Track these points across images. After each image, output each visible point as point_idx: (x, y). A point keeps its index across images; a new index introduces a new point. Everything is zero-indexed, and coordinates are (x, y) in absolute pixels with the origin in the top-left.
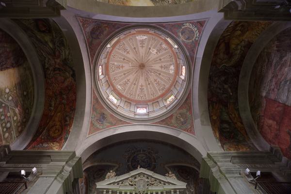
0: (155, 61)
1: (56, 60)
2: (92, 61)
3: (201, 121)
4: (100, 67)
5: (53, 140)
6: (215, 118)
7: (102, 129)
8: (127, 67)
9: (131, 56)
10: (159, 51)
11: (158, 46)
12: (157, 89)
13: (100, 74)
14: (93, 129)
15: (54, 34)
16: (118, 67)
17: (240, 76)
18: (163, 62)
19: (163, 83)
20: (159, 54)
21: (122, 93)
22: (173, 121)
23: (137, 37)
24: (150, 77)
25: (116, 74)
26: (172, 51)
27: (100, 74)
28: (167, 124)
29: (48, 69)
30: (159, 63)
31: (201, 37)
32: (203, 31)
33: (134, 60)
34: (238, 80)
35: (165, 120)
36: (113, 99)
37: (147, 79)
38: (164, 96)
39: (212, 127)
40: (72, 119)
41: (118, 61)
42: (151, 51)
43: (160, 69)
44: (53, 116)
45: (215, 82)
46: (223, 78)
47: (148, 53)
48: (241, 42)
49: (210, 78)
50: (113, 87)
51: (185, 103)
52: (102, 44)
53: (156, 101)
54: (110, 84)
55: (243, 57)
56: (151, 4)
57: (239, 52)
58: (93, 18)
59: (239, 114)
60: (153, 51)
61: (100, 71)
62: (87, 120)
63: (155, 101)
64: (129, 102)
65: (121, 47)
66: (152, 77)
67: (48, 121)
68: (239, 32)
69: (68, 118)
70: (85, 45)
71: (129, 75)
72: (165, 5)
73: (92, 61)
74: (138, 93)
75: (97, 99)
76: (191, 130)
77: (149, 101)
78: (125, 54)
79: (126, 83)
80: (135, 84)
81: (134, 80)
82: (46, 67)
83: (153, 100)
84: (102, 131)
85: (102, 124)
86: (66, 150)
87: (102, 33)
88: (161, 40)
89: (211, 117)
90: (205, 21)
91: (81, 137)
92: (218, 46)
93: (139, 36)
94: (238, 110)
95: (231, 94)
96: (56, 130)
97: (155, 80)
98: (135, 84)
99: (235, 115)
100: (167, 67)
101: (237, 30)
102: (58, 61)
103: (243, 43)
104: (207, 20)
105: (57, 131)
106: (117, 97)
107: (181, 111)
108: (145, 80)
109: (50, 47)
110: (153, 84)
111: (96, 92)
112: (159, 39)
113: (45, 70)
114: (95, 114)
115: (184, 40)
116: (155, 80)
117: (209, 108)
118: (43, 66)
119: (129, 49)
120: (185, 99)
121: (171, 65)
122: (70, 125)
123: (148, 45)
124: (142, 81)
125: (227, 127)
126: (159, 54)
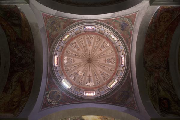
0: (79, 65)
1: (158, 75)
2: (129, 73)
3: (38, 27)
4: (123, 64)
5: (168, 10)
6: (26, 29)
7: (125, 17)
8: (102, 61)
9: (99, 69)
10: (77, 74)
11: (77, 78)
12: (77, 44)
13: (123, 58)
14: (132, 18)
15: (157, 97)
16: (108, 61)
17: (9, 63)
18: (73, 65)
19: (72, 48)
20: (76, 71)
21: (106, 40)
22: (62, 24)
23: (94, 84)
24: (83, 53)
25: (110, 56)
26: (66, 75)
27: (123, 58)
28: (68, 21)
29: (165, 69)
30: (76, 64)
31: (44, 95)
32: (43, 100)
33: (96, 66)
34: (10, 60)
35: (71, 23)
36: (114, 37)
37: (86, 50)
38: (71, 39)
39: (28, 22)
40: (150, 28)
41: (109, 66)
42: (83, 74)
43: (75, 59)
44: (165, 30)
45: (30, 59)
46: (23, 61)
47: (85, 71)
48: (12, 93)
49: (34, 62)
50: (113, 46)
51: (53, 40)
52: (121, 86)
53: (78, 35)
54: (116, 49)
55: (9, 80)
56: (85, 117)
57: (13, 84)
58: (126, 108)
59: (5, 32)
60: (81, 73)
61: (123, 61)
62: (137, 26)
63: (78, 34)
64: (101, 34)
65: (106, 77)
66: (81, 52)
67: (171, 25)
68: (15, 100)
69: (153, 28)
70: (134, 88)
71: (100, 54)
72: (74, 117)
73: (129, 73)
74: (93, 40)
75: (127, 42)
76: (47, 17)
77: (83, 34)
78: (103, 71)
79: (103, 48)
80: (96, 47)
81: (96, 50)
82: (166, 70)
83: (80, 35)
84: (124, 15)
85: (124, 22)
86: (156, 6)
87: (119, 97)
88: (75, 83)
89: (30, 30)
90: (43, 108)
91: (143, 14)
92: (30, 88)
93: (92, 85)
94: (7, 36)
95: (15, 49)
96: (165, 18)
97: (79, 50)
98: (96, 47)
99: (9, 31)
100: (69, 61)
101: (16, 102)
102: (156, 75)
103: (11, 91)
104: (41, 110)
105: (163, 17)
106: (112, 82)
107: (56, 33)
108: (87, 50)
109: (161, 86)
110: (81, 47)
111: (128, 47)
112: (77, 84)
113: (167, 68)
114: (129, 30)
115: (57, 91)
116: (79, 50)
117: (33, 37)
118: (168, 71)
119: (100, 74)
120: (53, 43)
121: (67, 64)
122: (152, 23)
123: (85, 78)
124: (90, 49)
125: (14, 21)
126: (76, 71)
